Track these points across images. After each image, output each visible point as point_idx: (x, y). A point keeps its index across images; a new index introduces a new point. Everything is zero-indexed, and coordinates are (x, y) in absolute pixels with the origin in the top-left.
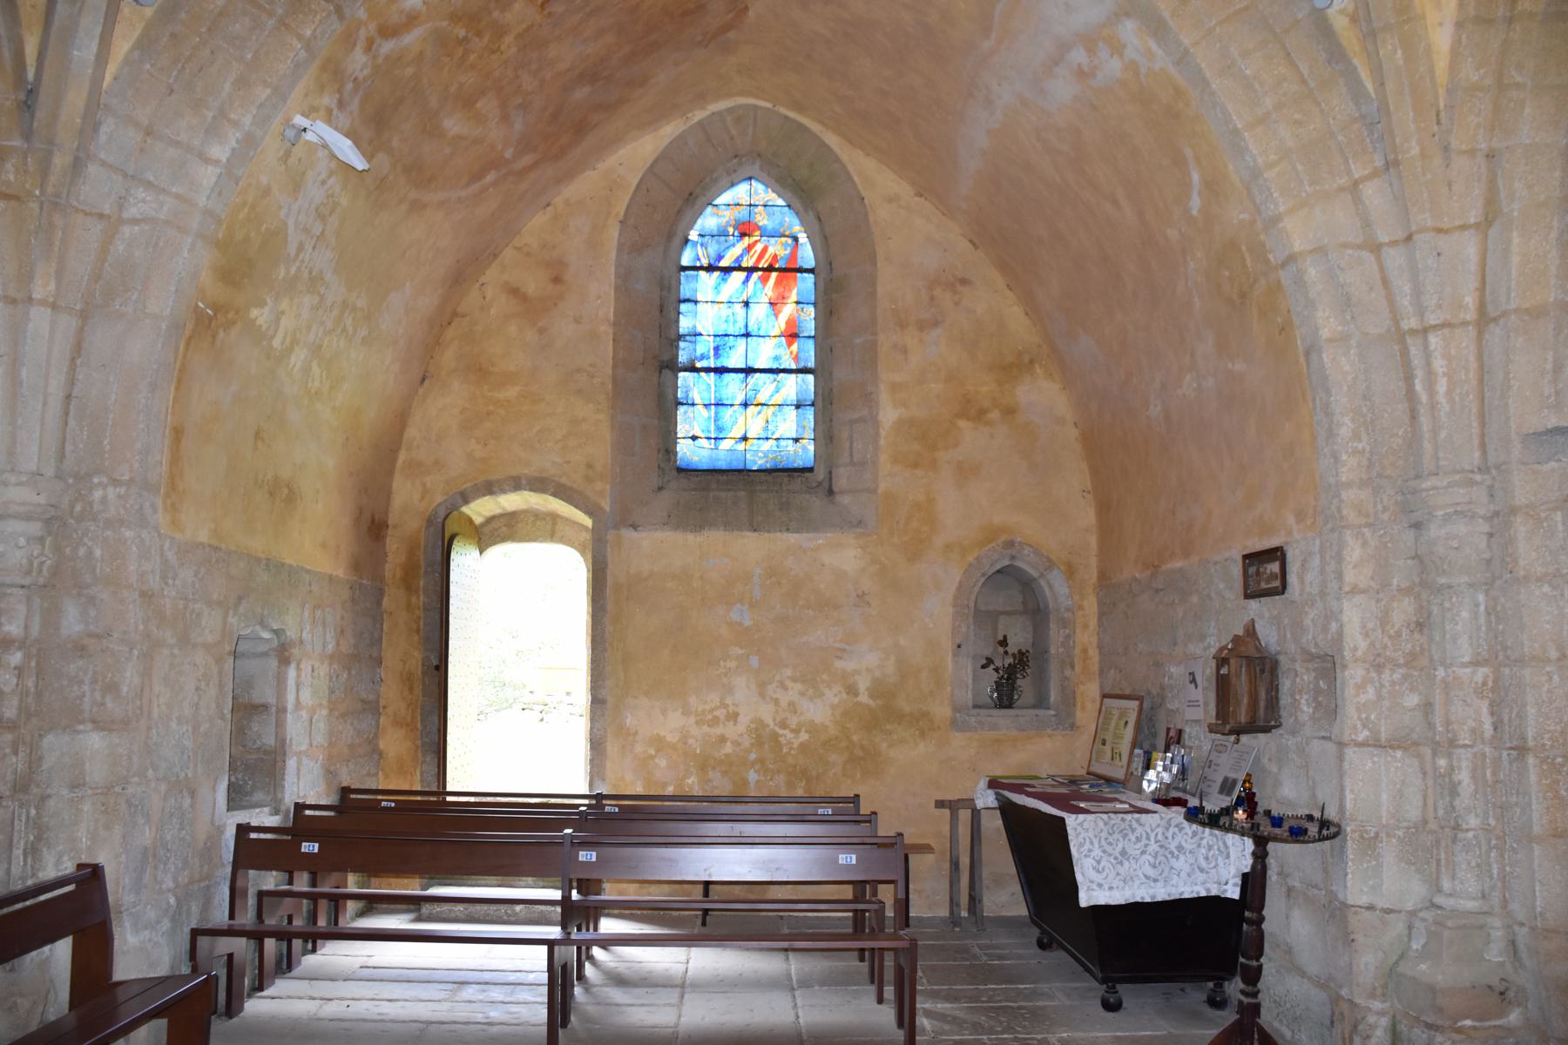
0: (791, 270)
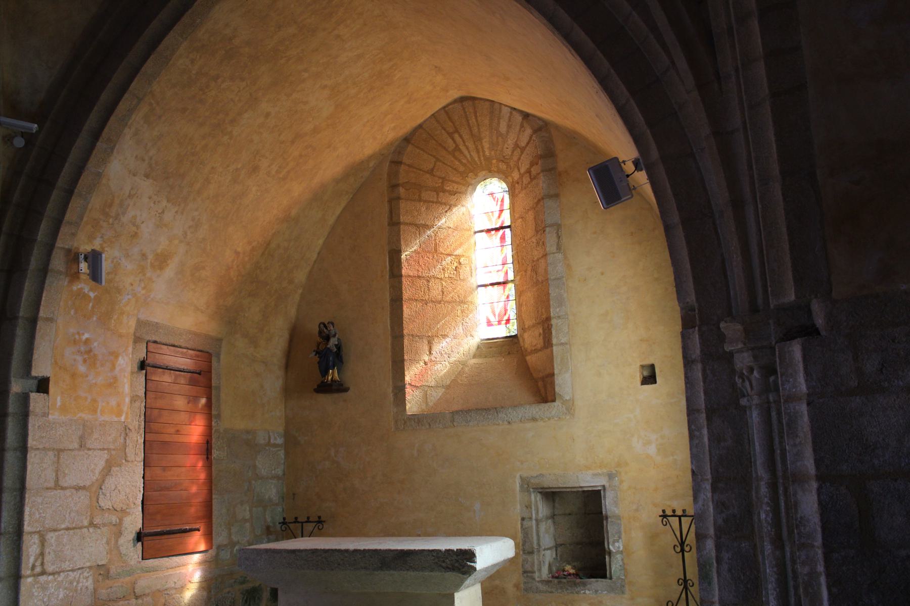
0: (504, 283)
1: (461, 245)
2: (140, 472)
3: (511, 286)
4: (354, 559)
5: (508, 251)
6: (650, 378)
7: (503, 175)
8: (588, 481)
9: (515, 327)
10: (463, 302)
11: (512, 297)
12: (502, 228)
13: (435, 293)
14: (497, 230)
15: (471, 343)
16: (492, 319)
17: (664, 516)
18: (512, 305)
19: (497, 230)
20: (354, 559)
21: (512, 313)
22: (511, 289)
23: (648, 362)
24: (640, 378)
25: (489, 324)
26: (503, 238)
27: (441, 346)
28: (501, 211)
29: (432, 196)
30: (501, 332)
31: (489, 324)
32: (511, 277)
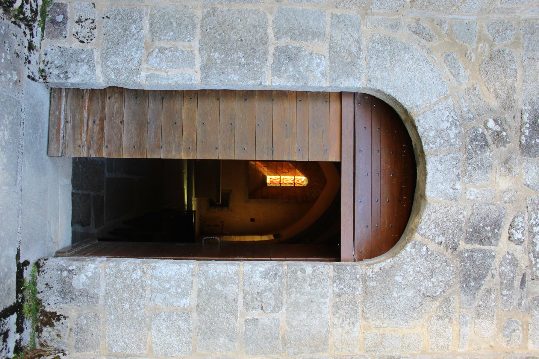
1: (291, 173)
2: (236, 87)
3: (279, 185)
4: (198, 20)
5: (288, 185)
6: (252, 220)
7: (308, 185)
8: (231, 205)
9: (269, 185)
10: (276, 173)
11: (276, 185)
12: (294, 184)
13: (279, 168)
14: (294, 182)
15: (266, 174)
16: (272, 179)
17: (223, 222)
18: (274, 185)
19: (294, 182)
20: (198, 20)
21: (272, 185)
22: (278, 185)
23: (255, 220)
24: (408, 225)
25: (271, 179)
26: (292, 184)
27: (266, 169)
28: (299, 184)
29: (125, 289)
30: (268, 181)
31: (271, 179)
32: (282, 185)
